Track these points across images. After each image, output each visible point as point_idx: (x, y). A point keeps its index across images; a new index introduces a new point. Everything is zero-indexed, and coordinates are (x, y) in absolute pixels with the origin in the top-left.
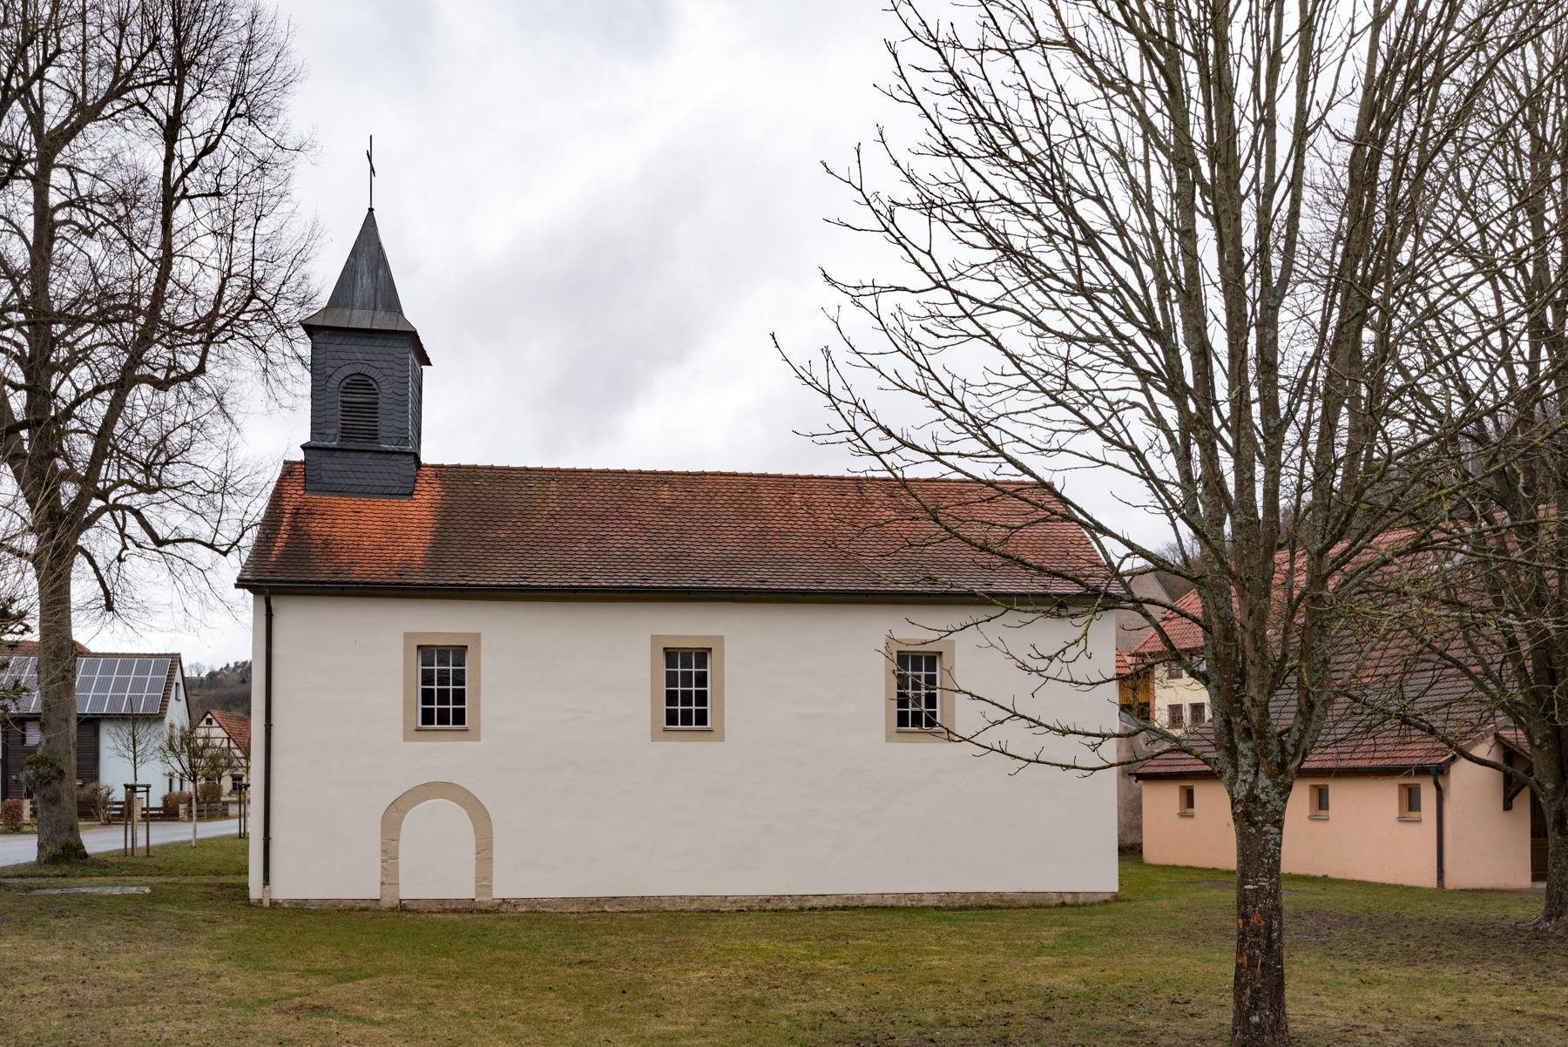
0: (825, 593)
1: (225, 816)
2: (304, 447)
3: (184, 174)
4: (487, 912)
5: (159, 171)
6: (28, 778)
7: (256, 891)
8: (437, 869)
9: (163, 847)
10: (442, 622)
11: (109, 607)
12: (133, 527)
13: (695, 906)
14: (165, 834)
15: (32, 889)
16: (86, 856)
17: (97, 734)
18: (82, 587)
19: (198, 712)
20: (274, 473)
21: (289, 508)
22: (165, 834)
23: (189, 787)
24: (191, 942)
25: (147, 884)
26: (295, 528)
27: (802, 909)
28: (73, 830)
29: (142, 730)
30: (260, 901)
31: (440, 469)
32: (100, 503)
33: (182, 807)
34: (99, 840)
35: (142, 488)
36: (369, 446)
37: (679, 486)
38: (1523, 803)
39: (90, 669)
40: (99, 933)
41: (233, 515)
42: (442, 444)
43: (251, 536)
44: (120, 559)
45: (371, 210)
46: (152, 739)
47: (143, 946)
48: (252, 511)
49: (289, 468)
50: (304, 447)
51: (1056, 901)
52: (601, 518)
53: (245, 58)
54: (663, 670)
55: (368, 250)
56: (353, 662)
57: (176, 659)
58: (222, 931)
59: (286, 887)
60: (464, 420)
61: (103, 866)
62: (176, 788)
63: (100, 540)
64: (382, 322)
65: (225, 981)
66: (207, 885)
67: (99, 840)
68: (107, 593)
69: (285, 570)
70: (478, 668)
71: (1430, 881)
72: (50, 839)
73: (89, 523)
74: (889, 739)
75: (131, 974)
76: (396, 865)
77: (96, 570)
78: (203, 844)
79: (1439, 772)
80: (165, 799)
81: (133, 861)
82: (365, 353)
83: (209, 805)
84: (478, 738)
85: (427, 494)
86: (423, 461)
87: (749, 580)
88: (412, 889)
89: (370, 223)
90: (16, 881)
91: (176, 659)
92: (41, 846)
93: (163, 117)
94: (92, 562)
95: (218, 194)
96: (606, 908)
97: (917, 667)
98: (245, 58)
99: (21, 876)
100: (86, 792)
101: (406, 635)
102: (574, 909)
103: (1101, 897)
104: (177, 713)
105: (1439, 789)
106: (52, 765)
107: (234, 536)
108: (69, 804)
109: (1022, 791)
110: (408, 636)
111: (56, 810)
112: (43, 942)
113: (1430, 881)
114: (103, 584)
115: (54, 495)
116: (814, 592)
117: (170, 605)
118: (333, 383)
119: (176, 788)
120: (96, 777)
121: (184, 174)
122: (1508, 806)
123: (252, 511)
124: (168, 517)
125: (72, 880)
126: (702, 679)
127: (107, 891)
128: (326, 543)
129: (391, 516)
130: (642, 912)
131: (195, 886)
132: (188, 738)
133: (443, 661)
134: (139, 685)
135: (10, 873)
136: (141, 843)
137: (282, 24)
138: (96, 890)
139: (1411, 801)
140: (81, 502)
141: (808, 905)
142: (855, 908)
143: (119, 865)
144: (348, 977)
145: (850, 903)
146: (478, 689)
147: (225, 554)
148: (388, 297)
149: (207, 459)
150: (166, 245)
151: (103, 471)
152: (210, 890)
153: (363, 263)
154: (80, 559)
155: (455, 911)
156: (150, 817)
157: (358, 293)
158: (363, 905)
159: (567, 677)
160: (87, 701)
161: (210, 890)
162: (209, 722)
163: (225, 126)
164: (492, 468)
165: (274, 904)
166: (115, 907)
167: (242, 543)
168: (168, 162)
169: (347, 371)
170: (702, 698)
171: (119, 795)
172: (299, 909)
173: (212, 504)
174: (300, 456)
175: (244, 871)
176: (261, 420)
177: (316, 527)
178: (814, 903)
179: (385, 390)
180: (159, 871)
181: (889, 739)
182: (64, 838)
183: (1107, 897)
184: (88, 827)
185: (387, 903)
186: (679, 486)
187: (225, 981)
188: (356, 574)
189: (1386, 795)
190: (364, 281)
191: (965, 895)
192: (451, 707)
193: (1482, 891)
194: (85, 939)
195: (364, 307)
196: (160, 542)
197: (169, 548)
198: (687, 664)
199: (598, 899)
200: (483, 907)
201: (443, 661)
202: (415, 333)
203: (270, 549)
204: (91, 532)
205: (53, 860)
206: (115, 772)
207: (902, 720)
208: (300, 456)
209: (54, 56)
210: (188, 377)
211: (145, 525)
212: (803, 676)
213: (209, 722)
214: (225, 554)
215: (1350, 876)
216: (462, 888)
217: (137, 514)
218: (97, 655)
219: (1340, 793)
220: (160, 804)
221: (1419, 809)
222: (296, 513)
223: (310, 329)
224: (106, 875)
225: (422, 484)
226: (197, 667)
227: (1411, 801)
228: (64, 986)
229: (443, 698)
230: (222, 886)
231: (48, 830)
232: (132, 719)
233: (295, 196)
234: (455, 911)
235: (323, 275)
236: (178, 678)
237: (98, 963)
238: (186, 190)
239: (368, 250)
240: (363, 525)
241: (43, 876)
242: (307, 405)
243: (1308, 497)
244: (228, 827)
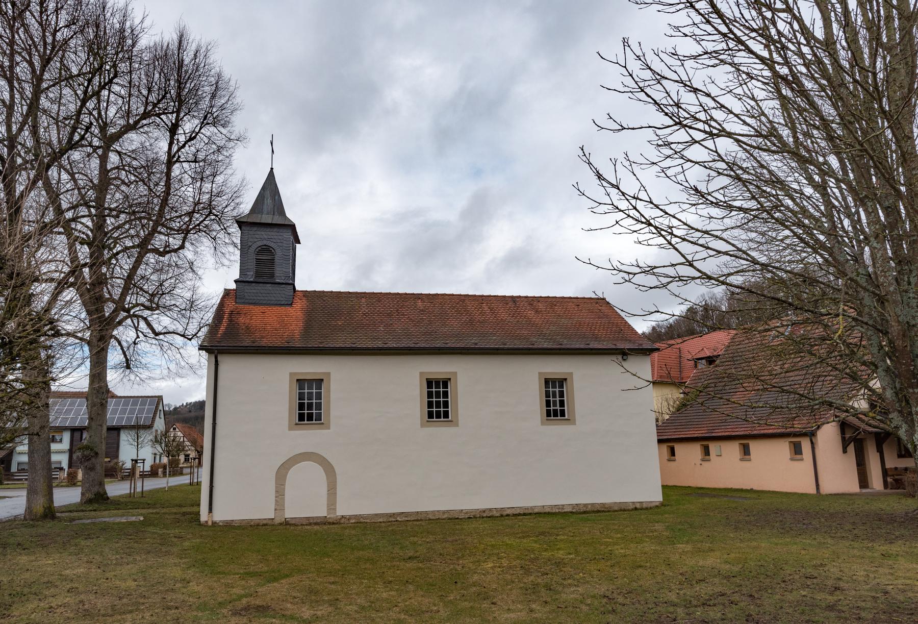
0: (508, 349)
1: (181, 474)
2: (236, 281)
3: (179, 150)
4: (333, 523)
5: (166, 149)
6: (78, 457)
7: (204, 516)
8: (306, 501)
9: (150, 491)
10: (309, 367)
11: (128, 367)
12: (143, 325)
13: (446, 516)
14: (151, 484)
15: (74, 520)
16: (108, 498)
17: (119, 435)
18: (114, 356)
19: (169, 425)
20: (221, 293)
21: (227, 311)
22: (151, 484)
23: (165, 460)
24: (168, 553)
25: (141, 515)
26: (230, 320)
27: (502, 516)
28: (101, 484)
29: (141, 432)
30: (207, 522)
31: (306, 293)
32: (125, 314)
33: (160, 470)
34: (116, 489)
35: (147, 308)
36: (269, 281)
37: (426, 300)
38: (851, 448)
39: (117, 404)
40: (110, 549)
41: (194, 321)
42: (303, 283)
43: (205, 330)
44: (135, 343)
46: (147, 437)
47: (138, 558)
48: (206, 318)
49: (227, 293)
50: (236, 281)
51: (632, 507)
52: (390, 315)
53: (213, 96)
54: (426, 390)
55: (270, 185)
56: (266, 385)
57: (160, 398)
58: (187, 544)
59: (222, 514)
60: (318, 269)
61: (118, 504)
62: (157, 461)
63: (125, 333)
64: (277, 220)
65: (193, 587)
66: (176, 514)
67: (116, 489)
68: (127, 360)
69: (228, 338)
70: (329, 391)
71: (813, 491)
72: (88, 490)
73: (120, 323)
74: (543, 423)
75: (131, 584)
76: (284, 499)
77: (122, 348)
78: (172, 489)
79: (812, 435)
80: (152, 467)
81: (134, 500)
82: (268, 235)
83: (174, 469)
84: (329, 428)
85: (299, 305)
86: (297, 288)
87: (469, 343)
88: (292, 512)
89: (271, 174)
90: (67, 514)
91: (160, 398)
92: (83, 494)
93: (170, 124)
94: (120, 343)
95: (195, 161)
96: (398, 519)
98: (213, 96)
99: (70, 511)
100: (112, 464)
101: (291, 374)
102: (381, 520)
103: (654, 504)
104: (160, 424)
105: (812, 443)
106: (92, 450)
107: (195, 331)
108: (100, 469)
109: (614, 449)
111: (92, 474)
112: (74, 558)
113: (813, 491)
114: (125, 356)
115: (100, 310)
116: (503, 349)
117: (160, 366)
118: (252, 250)
119: (157, 461)
120: (117, 457)
121: (179, 150)
122: (845, 451)
123: (206, 318)
124: (162, 321)
125: (98, 513)
126: (446, 394)
127: (118, 520)
128: (248, 328)
129: (277, 319)
130: (417, 520)
131: (169, 514)
132: (166, 434)
134: (141, 411)
135: (64, 509)
136: (139, 489)
137: (232, 83)
138: (112, 519)
139: (797, 450)
140: (116, 312)
141: (505, 513)
142: (530, 514)
143: (126, 504)
144: (274, 577)
145: (526, 512)
146: (329, 402)
147: (190, 340)
148: (279, 208)
149: (183, 293)
150: (168, 185)
151: (128, 298)
152: (177, 516)
153: (268, 193)
154: (113, 342)
155: (316, 524)
156: (143, 476)
157: (265, 207)
158: (265, 522)
159: (373, 394)
160: (113, 416)
161: (177, 516)
162: (174, 429)
163: (201, 128)
164: (332, 292)
165: (214, 524)
166: (122, 530)
167: (200, 334)
168: (171, 145)
169: (259, 244)
170: (446, 404)
171: (129, 465)
172: (229, 527)
173: (183, 316)
174: (233, 286)
176: (213, 272)
177: (241, 320)
178: (508, 512)
179: (279, 253)
180: (149, 506)
181: (543, 423)
182: (96, 489)
183: (657, 504)
184: (111, 482)
185: (277, 521)
186: (426, 300)
187: (193, 587)
188: (264, 342)
189: (783, 448)
190: (268, 202)
191: (585, 505)
193: (838, 494)
194: (101, 553)
195: (268, 214)
196: (157, 334)
197: (161, 337)
199: (394, 514)
200: (331, 521)
202: (294, 225)
203: (217, 331)
204: (121, 328)
205: (90, 501)
206: (127, 452)
207: (548, 414)
208: (233, 286)
209: (113, 78)
210: (176, 251)
211: (149, 325)
212: (494, 392)
213: (174, 429)
214: (190, 340)
215: (768, 489)
216: (320, 511)
217: (145, 319)
218: (121, 397)
219: (756, 447)
220: (149, 469)
221: (801, 454)
222: (231, 313)
223: (241, 223)
224: (119, 509)
225: (297, 300)
226: (169, 405)
227: (797, 450)
228: (82, 597)
229: (308, 409)
230: (184, 514)
231: (87, 485)
232: (137, 428)
233: (234, 166)
234: (316, 524)
235: (246, 204)
236: (161, 407)
237: (108, 575)
238: (179, 157)
239: (270, 185)
240: (264, 319)
241: (83, 511)
242: (238, 265)
244: (184, 480)
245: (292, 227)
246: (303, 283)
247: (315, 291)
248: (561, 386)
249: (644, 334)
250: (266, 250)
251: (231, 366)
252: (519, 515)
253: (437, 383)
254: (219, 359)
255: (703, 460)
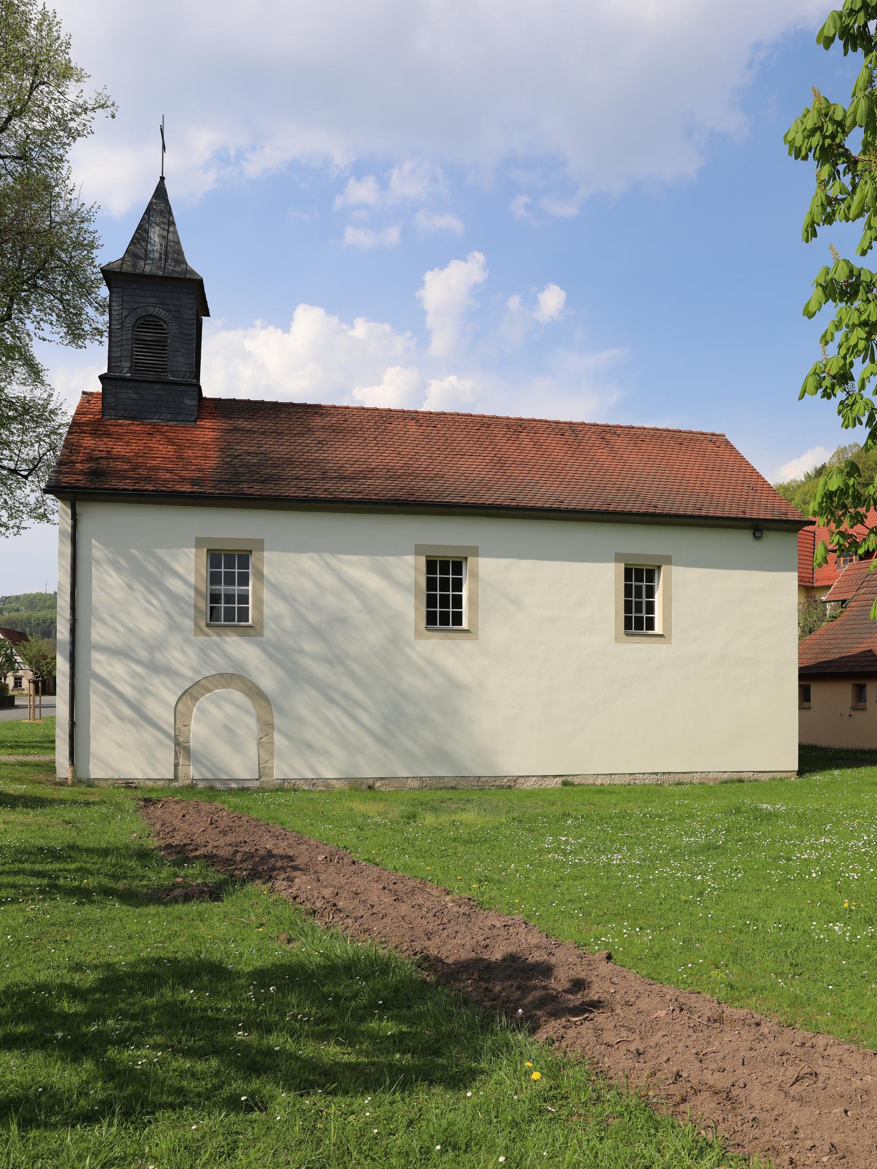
2: (102, 378)
42: (213, 385)
45: (162, 178)
50: (102, 378)
86: (206, 393)
89: (161, 193)
97: (639, 579)
110: (418, 635)
133: (230, 564)
175: (49, 744)
181: (617, 639)
190: (155, 235)
192: (438, 593)
198: (444, 571)
201: (230, 564)
229: (226, 598)
243: (10, 681)
245: (196, 286)
246: (213, 385)
247: (234, 400)
248: (651, 578)
249: (422, 284)
250: (149, 323)
251: (100, 519)
252: (732, 781)
253: (444, 565)
254: (78, 510)
255: (854, 709)
